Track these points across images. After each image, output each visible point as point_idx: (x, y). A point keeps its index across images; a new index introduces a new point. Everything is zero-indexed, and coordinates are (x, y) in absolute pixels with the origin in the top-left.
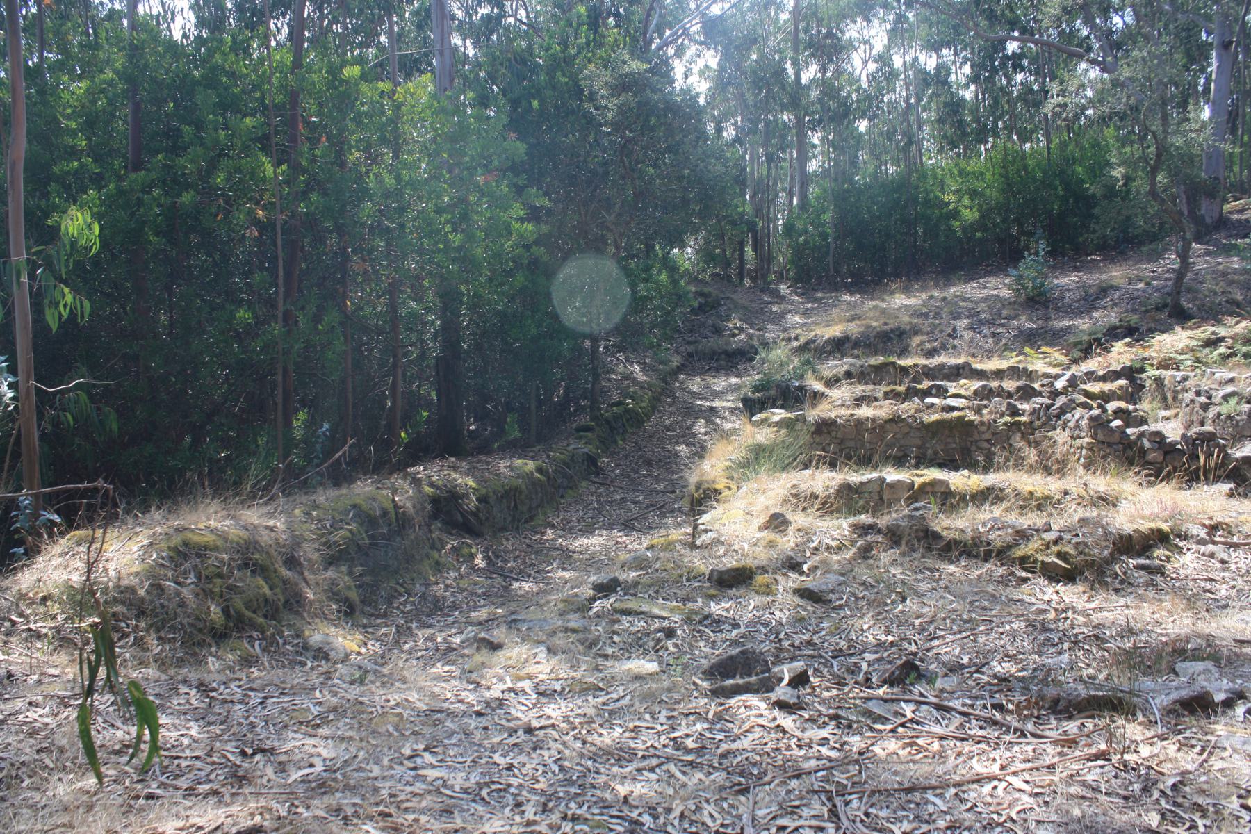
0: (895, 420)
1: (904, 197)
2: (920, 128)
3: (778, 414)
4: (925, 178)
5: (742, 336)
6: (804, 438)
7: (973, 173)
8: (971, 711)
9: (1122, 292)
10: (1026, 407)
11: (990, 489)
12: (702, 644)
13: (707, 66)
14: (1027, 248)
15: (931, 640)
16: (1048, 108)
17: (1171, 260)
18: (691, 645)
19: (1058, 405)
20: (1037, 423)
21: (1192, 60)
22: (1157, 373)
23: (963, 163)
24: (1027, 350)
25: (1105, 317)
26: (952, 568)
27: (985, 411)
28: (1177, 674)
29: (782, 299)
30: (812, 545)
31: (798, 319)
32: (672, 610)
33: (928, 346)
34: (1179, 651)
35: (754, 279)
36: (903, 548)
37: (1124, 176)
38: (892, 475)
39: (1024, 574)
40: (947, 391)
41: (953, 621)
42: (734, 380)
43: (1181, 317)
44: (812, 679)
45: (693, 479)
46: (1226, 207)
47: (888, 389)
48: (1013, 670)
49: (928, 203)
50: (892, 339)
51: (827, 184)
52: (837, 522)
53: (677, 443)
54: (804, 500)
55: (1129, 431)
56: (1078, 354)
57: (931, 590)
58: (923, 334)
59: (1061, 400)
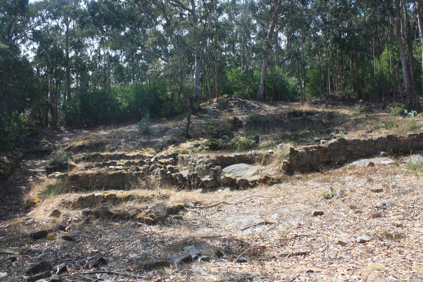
0: (99, 174)
1: (104, 98)
2: (109, 75)
3: (58, 174)
4: (111, 92)
5: (47, 145)
6: (67, 181)
7: (126, 91)
8: (119, 273)
9: (172, 130)
10: (142, 168)
11: (130, 196)
12: (27, 262)
13: (34, 48)
14: (144, 116)
15: (110, 249)
16: (149, 72)
17: (185, 120)
18: (22, 262)
19: (151, 167)
20: (145, 173)
21: (190, 61)
22: (182, 155)
23: (123, 88)
24: (143, 149)
25: (167, 138)
26: (117, 224)
27: (129, 170)
28: (184, 251)
29: (62, 132)
30: (69, 220)
31: (67, 139)
32: (15, 250)
33: (112, 148)
34: (186, 243)
35: (51, 125)
36: (100, 218)
37: (171, 94)
38: (97, 193)
39: (140, 224)
40: (116, 164)
41: (117, 242)
42: (43, 161)
43: (188, 138)
44: (68, 269)
45: (26, 199)
46: (201, 105)
47: (96, 163)
48: (136, 256)
49: (111, 100)
50: (99, 146)
51: (78, 92)
52: (78, 211)
53: (21, 185)
54: (66, 204)
55: (172, 174)
56: (158, 150)
57: (110, 232)
58: (110, 144)
59: (153, 165)
